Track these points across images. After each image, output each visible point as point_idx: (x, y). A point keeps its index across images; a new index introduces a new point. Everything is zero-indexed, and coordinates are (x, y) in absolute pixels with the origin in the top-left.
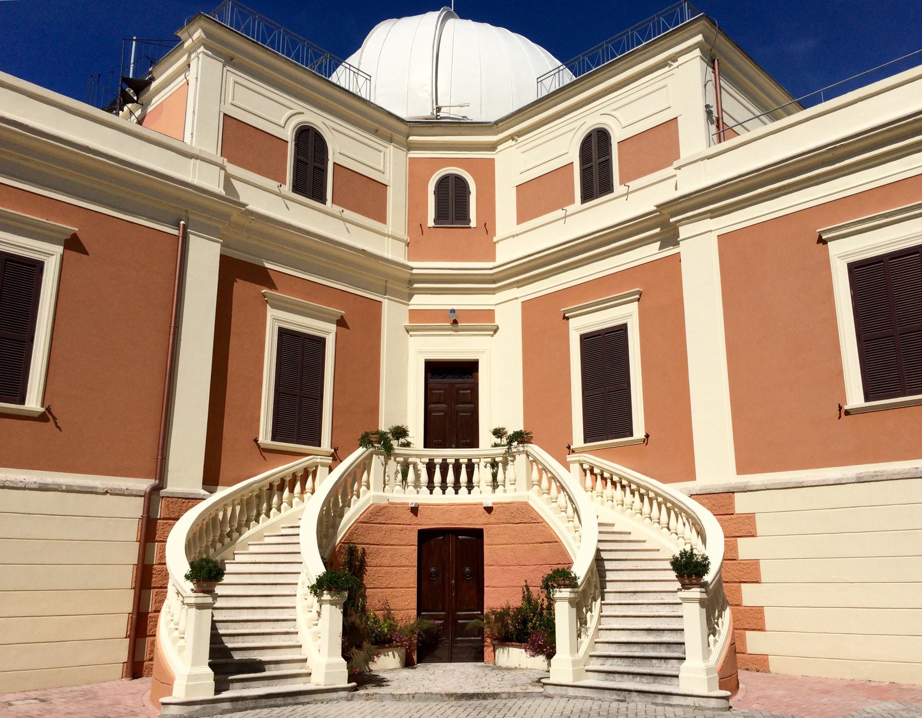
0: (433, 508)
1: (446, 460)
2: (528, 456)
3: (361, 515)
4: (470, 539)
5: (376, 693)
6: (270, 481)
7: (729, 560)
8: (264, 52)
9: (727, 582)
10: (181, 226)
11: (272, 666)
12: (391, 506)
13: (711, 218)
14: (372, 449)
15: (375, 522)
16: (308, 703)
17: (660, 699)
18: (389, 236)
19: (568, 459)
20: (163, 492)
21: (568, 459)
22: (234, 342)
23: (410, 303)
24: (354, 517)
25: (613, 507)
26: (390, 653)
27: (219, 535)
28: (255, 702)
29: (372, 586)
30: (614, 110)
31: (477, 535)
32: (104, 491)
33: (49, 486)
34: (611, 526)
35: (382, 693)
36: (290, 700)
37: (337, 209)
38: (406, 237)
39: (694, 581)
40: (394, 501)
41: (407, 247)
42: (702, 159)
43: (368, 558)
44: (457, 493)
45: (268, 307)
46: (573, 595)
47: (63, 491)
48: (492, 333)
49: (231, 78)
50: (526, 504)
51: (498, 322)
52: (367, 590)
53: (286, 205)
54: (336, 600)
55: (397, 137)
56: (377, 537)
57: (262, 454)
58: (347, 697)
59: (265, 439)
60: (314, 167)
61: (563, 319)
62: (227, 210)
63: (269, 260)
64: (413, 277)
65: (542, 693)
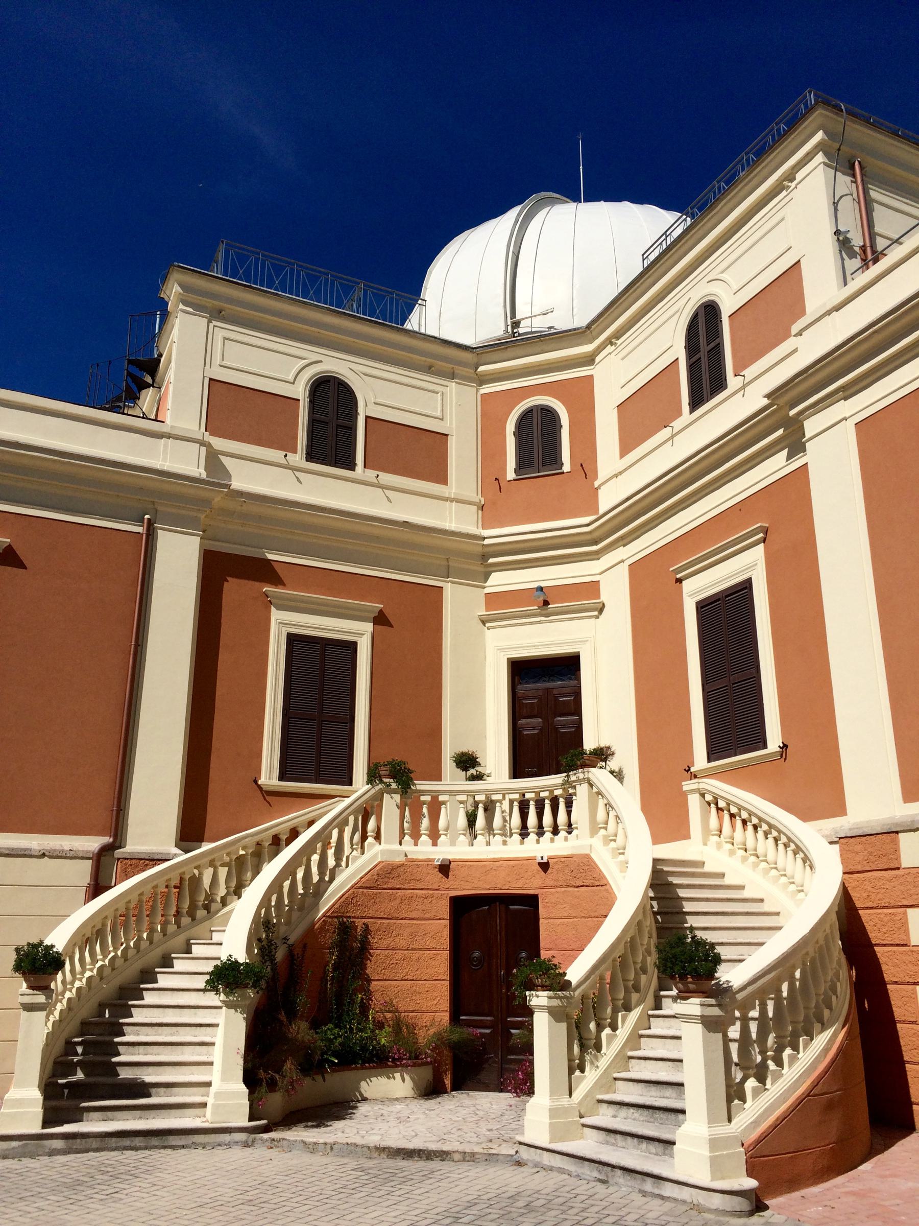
0: (471, 866)
1: (524, 795)
2: (591, 785)
3: (361, 878)
4: (524, 910)
5: (283, 1139)
6: (274, 834)
7: (898, 945)
8: (263, 296)
9: (896, 983)
10: (146, 521)
11: (162, 1090)
12: (408, 863)
13: (846, 399)
14: (380, 786)
15: (385, 887)
16: (183, 1147)
17: (649, 1185)
18: (452, 500)
19: (685, 788)
20: (118, 853)
21: (685, 788)
22: (225, 658)
23: (486, 585)
24: (350, 881)
25: (744, 859)
26: (397, 1075)
27: (187, 907)
28: (102, 1141)
29: (381, 977)
30: (723, 272)
31: (532, 901)
32: (41, 853)
34: (739, 889)
35: (291, 1139)
36: (155, 1141)
37: (371, 474)
38: (479, 498)
39: (692, 986)
40: (414, 857)
41: (480, 512)
42: (829, 313)
43: (373, 938)
44: (435, 844)
45: (273, 609)
46: (556, 1003)
48: (596, 613)
49: (220, 334)
50: (587, 857)
51: (604, 598)
52: (373, 982)
53: (297, 477)
54: (234, 1001)
55: (459, 370)
56: (387, 907)
57: (265, 799)
58: (246, 1142)
59: (270, 779)
60: (337, 425)
61: (676, 583)
62: (206, 495)
63: (272, 549)
64: (487, 550)
65: (512, 1156)
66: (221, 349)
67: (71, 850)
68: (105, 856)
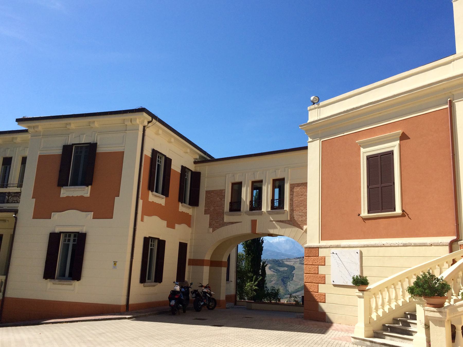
32: (430, 244)
33: (407, 244)
47: (413, 246)
59: (364, 214)
66: (14, 188)
67: (441, 243)
68: (454, 244)
